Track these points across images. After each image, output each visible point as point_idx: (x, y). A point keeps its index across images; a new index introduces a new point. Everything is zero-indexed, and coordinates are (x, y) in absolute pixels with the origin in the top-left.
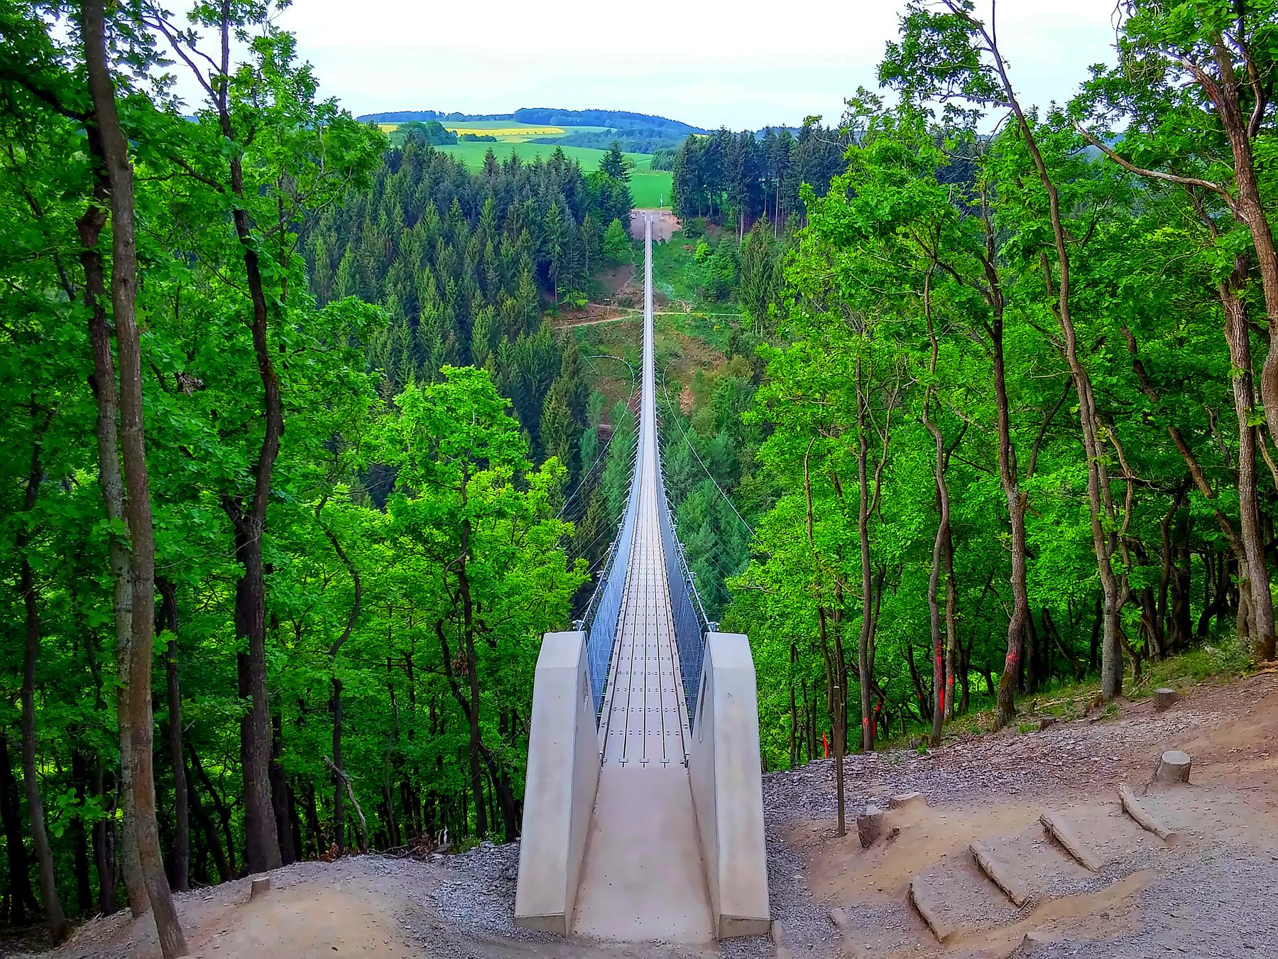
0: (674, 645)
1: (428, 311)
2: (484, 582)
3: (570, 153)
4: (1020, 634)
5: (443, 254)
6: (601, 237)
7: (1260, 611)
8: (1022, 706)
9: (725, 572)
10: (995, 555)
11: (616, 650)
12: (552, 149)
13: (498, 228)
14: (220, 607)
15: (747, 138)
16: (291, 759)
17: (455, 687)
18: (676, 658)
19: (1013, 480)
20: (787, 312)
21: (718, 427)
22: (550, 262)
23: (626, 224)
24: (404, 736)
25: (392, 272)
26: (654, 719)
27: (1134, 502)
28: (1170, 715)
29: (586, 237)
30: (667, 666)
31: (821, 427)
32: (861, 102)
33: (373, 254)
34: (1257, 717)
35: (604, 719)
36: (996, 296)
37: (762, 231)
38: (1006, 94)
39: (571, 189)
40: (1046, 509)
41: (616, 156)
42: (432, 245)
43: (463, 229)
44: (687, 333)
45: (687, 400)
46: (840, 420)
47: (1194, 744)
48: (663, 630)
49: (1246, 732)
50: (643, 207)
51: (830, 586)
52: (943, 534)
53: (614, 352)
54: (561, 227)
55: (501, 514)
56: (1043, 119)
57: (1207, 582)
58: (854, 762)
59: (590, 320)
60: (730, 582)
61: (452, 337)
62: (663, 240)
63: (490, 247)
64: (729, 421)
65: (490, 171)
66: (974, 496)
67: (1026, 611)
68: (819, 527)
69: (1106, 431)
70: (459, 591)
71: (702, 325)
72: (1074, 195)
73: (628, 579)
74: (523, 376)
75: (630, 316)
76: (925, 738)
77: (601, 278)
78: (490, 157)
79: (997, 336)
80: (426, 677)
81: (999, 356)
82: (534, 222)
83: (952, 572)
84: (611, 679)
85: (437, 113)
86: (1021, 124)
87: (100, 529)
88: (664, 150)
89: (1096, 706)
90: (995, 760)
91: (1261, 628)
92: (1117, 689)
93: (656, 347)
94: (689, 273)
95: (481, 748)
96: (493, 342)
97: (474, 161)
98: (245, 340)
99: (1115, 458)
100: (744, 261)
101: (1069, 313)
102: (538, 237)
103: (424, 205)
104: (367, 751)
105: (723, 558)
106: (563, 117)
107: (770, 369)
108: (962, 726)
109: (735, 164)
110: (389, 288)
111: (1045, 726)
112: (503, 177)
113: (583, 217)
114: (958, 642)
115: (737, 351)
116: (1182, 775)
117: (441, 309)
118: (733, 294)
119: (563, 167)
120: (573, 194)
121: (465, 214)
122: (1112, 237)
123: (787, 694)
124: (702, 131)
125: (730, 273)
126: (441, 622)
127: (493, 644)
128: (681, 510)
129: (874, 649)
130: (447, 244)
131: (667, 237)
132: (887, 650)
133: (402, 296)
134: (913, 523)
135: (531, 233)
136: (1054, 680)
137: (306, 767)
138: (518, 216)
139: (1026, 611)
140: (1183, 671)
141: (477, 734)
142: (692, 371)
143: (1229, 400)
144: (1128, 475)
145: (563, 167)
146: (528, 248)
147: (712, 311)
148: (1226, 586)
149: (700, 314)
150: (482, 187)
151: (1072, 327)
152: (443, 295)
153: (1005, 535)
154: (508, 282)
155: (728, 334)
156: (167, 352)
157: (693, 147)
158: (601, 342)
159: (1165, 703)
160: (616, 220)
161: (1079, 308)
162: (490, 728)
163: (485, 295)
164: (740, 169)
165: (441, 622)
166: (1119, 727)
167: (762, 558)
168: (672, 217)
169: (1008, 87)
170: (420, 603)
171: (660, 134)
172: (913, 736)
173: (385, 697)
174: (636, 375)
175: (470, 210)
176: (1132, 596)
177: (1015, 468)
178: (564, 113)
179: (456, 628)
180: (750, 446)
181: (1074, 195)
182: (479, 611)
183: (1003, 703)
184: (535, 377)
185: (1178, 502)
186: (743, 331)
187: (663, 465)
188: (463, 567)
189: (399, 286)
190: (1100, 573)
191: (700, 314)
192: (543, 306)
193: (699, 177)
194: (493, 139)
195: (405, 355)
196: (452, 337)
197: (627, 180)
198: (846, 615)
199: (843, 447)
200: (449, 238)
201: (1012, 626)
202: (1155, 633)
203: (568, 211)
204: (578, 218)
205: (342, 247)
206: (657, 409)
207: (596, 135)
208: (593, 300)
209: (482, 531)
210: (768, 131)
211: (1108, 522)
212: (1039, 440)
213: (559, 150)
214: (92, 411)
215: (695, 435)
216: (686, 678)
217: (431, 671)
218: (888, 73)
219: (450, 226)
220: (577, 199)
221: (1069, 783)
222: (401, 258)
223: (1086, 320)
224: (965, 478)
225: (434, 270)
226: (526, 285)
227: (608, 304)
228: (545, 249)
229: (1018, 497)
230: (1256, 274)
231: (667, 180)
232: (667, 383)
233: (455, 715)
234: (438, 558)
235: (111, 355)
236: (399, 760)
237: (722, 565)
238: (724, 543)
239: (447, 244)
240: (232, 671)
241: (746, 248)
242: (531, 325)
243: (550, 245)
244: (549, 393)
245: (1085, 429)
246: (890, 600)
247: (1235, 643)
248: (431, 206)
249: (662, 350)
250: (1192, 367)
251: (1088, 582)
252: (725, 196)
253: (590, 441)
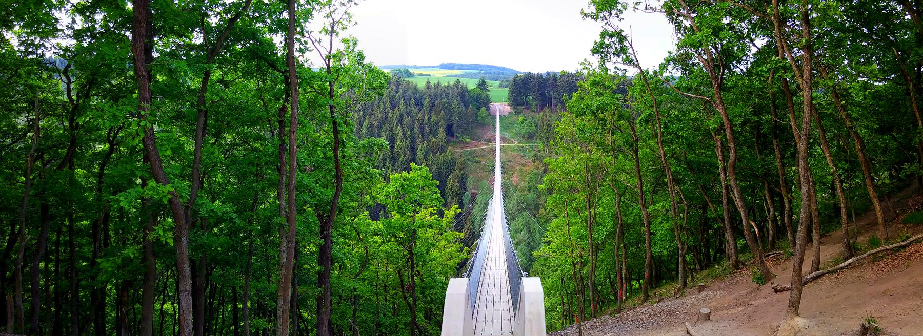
0: (508, 282)
1: (399, 143)
2: (421, 256)
3: (462, 80)
4: (650, 266)
5: (406, 120)
6: (477, 114)
7: (733, 252)
8: (651, 293)
9: (533, 249)
10: (640, 234)
11: (480, 285)
12: (455, 79)
13: (430, 110)
14: (312, 253)
15: (539, 77)
16: (334, 317)
17: (405, 298)
18: (509, 288)
19: (645, 206)
20: (558, 144)
21: (529, 190)
23: (488, 109)
24: (381, 315)
25: (384, 127)
26: (497, 314)
27: (688, 213)
28: (703, 293)
29: (470, 114)
30: (504, 291)
31: (572, 189)
32: (584, 64)
33: (377, 120)
34: (733, 292)
35: (475, 315)
36: (635, 138)
37: (547, 112)
38: (636, 63)
39: (463, 95)
40: (657, 217)
41: (483, 82)
42: (402, 117)
43: (415, 111)
45: (515, 179)
46: (579, 187)
47: (712, 304)
48: (503, 276)
49: (730, 298)
50: (495, 102)
51: (576, 253)
52: (620, 229)
53: (483, 161)
54: (458, 110)
55: (431, 227)
56: (651, 73)
57: (716, 241)
58: (587, 324)
60: (534, 253)
61: (408, 154)
62: (504, 115)
63: (426, 118)
65: (428, 88)
66: (631, 213)
67: (652, 256)
68: (572, 229)
69: (677, 188)
70: (409, 258)
71: (522, 149)
72: (662, 102)
73: (487, 255)
74: (438, 170)
75: (490, 145)
76: (615, 310)
77: (476, 131)
78: (428, 83)
79: (637, 153)
80: (392, 292)
81: (637, 160)
82: (446, 108)
83: (624, 243)
84: (478, 298)
86: (643, 74)
87: (276, 220)
88: (505, 80)
89: (678, 291)
90: (641, 316)
91: (733, 258)
92: (685, 285)
93: (502, 158)
94: (516, 128)
95: (416, 324)
96: (426, 157)
97: (421, 84)
98: (331, 154)
99: (681, 198)
100: (539, 123)
101: (662, 144)
102: (448, 115)
103: (399, 101)
104: (366, 319)
105: (532, 244)
106: (460, 67)
107: (550, 167)
108: (629, 303)
109: (535, 86)
111: (659, 301)
112: (433, 90)
113: (469, 106)
114: (627, 269)
115: (537, 159)
116: (708, 317)
117: (404, 142)
118: (535, 137)
119: (460, 86)
120: (464, 97)
121: (417, 105)
122: (676, 116)
123: (560, 298)
124: (521, 73)
125: (534, 128)
126: (400, 270)
127: (422, 281)
128: (513, 225)
129: (595, 276)
130: (408, 116)
131: (506, 114)
132: (600, 276)
134: (609, 225)
135: (445, 113)
136: (664, 282)
137: (340, 322)
139: (652, 256)
140: (708, 276)
141: (414, 318)
142: (518, 168)
143: (719, 175)
144: (685, 203)
145: (460, 86)
146: (444, 118)
148: (721, 243)
150: (424, 94)
151: (663, 149)
152: (405, 137)
153: (642, 228)
154: (433, 132)
155: (533, 153)
156: (303, 157)
157: (517, 79)
158: (476, 156)
159: (702, 289)
160: (483, 108)
161: (665, 142)
162: (420, 316)
163: (423, 137)
164: (537, 88)
165: (400, 270)
166: (686, 300)
167: (548, 243)
168: (508, 107)
169: (637, 61)
170: (392, 262)
171: (503, 74)
172: (611, 309)
173: (374, 298)
174: (492, 170)
175: (419, 103)
176: (689, 248)
177: (645, 202)
178: (489, 65)
179: (407, 273)
180: (543, 197)
181: (662, 102)
182: (417, 266)
183: (644, 293)
185: (703, 212)
186: (540, 151)
187: (505, 206)
188: (411, 248)
189: (387, 133)
190: (677, 241)
192: (448, 142)
193: (520, 91)
194: (430, 75)
195: (388, 161)
196: (408, 154)
197: (488, 91)
198: (583, 264)
199: (581, 196)
200: (409, 114)
201: (646, 263)
202: (698, 262)
203: (462, 104)
204: (466, 105)
205: (365, 118)
206: (502, 184)
207: (474, 73)
208: (473, 140)
209: (421, 232)
210: (548, 73)
211: (679, 222)
212: (653, 191)
213: (458, 80)
214: (277, 178)
215: (519, 193)
216: (513, 296)
217: (395, 290)
218: (595, 51)
219: (410, 109)
220: (466, 99)
221: (668, 323)
222: (388, 122)
223: (668, 146)
224: (627, 206)
225: (402, 127)
226: (441, 133)
227: (480, 141)
229: (647, 213)
230: (724, 130)
231: (506, 92)
232: (506, 173)
233: (404, 309)
234: (401, 244)
235: (286, 158)
236: (379, 325)
237: (531, 246)
238: (533, 237)
239: (408, 116)
240: (315, 279)
241: (540, 119)
242: (443, 149)
245: (669, 187)
246: (601, 256)
247: (725, 264)
248: (402, 102)
249: (505, 160)
250: (706, 163)
251: (672, 244)
252: (531, 98)
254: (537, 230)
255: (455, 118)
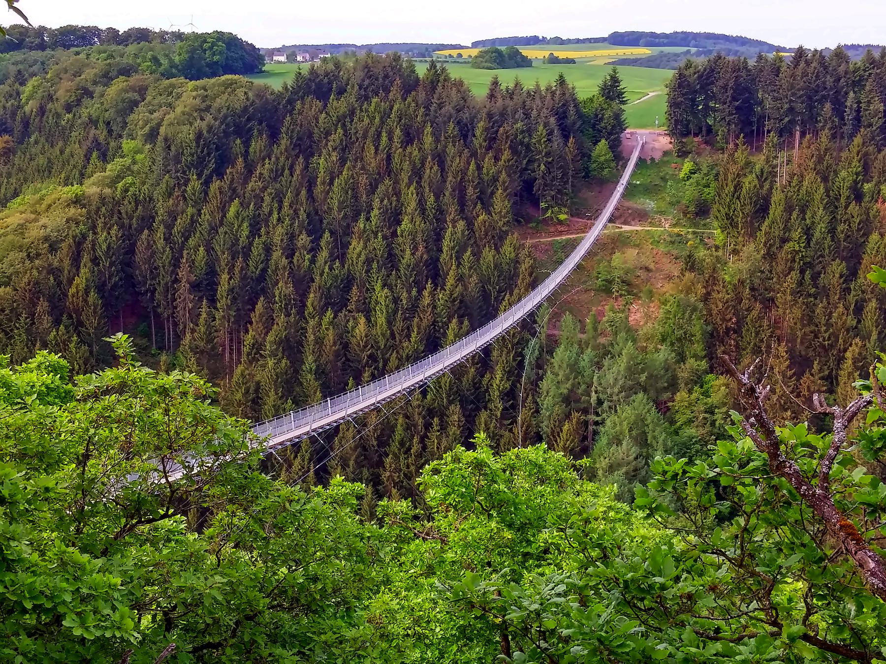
1: (406, 224)
5: (431, 171)
22: (536, 179)
25: (381, 189)
39: (565, 112)
44: (662, 248)
59: (571, 234)
61: (421, 248)
62: (653, 159)
64: (673, 337)
82: (522, 143)
85: (541, 38)
109: (725, 88)
110: (376, 203)
124: (784, 49)
133: (387, 210)
138: (507, 137)
147: (690, 227)
149: (676, 230)
157: (687, 73)
164: (730, 92)
175: (465, 132)
178: (653, 35)
184: (495, 288)
189: (386, 201)
191: (676, 230)
195: (375, 265)
196: (421, 248)
200: (440, 159)
210: (800, 53)
220: (569, 121)
226: (501, 203)
228: (530, 167)
243: (536, 165)
244: (504, 304)
248: (428, 129)
253: (534, 350)
254: (661, 441)
255: (539, 166)
